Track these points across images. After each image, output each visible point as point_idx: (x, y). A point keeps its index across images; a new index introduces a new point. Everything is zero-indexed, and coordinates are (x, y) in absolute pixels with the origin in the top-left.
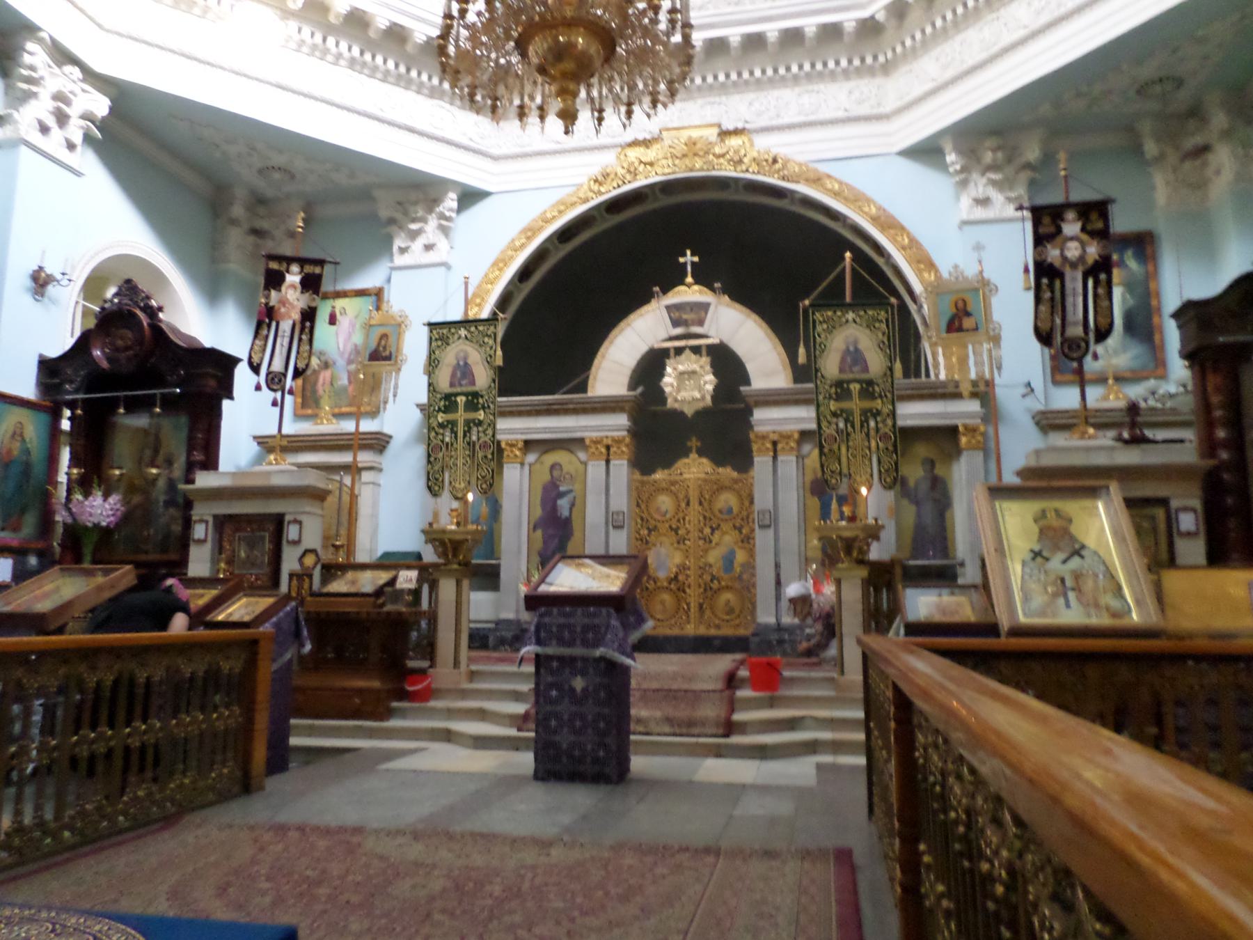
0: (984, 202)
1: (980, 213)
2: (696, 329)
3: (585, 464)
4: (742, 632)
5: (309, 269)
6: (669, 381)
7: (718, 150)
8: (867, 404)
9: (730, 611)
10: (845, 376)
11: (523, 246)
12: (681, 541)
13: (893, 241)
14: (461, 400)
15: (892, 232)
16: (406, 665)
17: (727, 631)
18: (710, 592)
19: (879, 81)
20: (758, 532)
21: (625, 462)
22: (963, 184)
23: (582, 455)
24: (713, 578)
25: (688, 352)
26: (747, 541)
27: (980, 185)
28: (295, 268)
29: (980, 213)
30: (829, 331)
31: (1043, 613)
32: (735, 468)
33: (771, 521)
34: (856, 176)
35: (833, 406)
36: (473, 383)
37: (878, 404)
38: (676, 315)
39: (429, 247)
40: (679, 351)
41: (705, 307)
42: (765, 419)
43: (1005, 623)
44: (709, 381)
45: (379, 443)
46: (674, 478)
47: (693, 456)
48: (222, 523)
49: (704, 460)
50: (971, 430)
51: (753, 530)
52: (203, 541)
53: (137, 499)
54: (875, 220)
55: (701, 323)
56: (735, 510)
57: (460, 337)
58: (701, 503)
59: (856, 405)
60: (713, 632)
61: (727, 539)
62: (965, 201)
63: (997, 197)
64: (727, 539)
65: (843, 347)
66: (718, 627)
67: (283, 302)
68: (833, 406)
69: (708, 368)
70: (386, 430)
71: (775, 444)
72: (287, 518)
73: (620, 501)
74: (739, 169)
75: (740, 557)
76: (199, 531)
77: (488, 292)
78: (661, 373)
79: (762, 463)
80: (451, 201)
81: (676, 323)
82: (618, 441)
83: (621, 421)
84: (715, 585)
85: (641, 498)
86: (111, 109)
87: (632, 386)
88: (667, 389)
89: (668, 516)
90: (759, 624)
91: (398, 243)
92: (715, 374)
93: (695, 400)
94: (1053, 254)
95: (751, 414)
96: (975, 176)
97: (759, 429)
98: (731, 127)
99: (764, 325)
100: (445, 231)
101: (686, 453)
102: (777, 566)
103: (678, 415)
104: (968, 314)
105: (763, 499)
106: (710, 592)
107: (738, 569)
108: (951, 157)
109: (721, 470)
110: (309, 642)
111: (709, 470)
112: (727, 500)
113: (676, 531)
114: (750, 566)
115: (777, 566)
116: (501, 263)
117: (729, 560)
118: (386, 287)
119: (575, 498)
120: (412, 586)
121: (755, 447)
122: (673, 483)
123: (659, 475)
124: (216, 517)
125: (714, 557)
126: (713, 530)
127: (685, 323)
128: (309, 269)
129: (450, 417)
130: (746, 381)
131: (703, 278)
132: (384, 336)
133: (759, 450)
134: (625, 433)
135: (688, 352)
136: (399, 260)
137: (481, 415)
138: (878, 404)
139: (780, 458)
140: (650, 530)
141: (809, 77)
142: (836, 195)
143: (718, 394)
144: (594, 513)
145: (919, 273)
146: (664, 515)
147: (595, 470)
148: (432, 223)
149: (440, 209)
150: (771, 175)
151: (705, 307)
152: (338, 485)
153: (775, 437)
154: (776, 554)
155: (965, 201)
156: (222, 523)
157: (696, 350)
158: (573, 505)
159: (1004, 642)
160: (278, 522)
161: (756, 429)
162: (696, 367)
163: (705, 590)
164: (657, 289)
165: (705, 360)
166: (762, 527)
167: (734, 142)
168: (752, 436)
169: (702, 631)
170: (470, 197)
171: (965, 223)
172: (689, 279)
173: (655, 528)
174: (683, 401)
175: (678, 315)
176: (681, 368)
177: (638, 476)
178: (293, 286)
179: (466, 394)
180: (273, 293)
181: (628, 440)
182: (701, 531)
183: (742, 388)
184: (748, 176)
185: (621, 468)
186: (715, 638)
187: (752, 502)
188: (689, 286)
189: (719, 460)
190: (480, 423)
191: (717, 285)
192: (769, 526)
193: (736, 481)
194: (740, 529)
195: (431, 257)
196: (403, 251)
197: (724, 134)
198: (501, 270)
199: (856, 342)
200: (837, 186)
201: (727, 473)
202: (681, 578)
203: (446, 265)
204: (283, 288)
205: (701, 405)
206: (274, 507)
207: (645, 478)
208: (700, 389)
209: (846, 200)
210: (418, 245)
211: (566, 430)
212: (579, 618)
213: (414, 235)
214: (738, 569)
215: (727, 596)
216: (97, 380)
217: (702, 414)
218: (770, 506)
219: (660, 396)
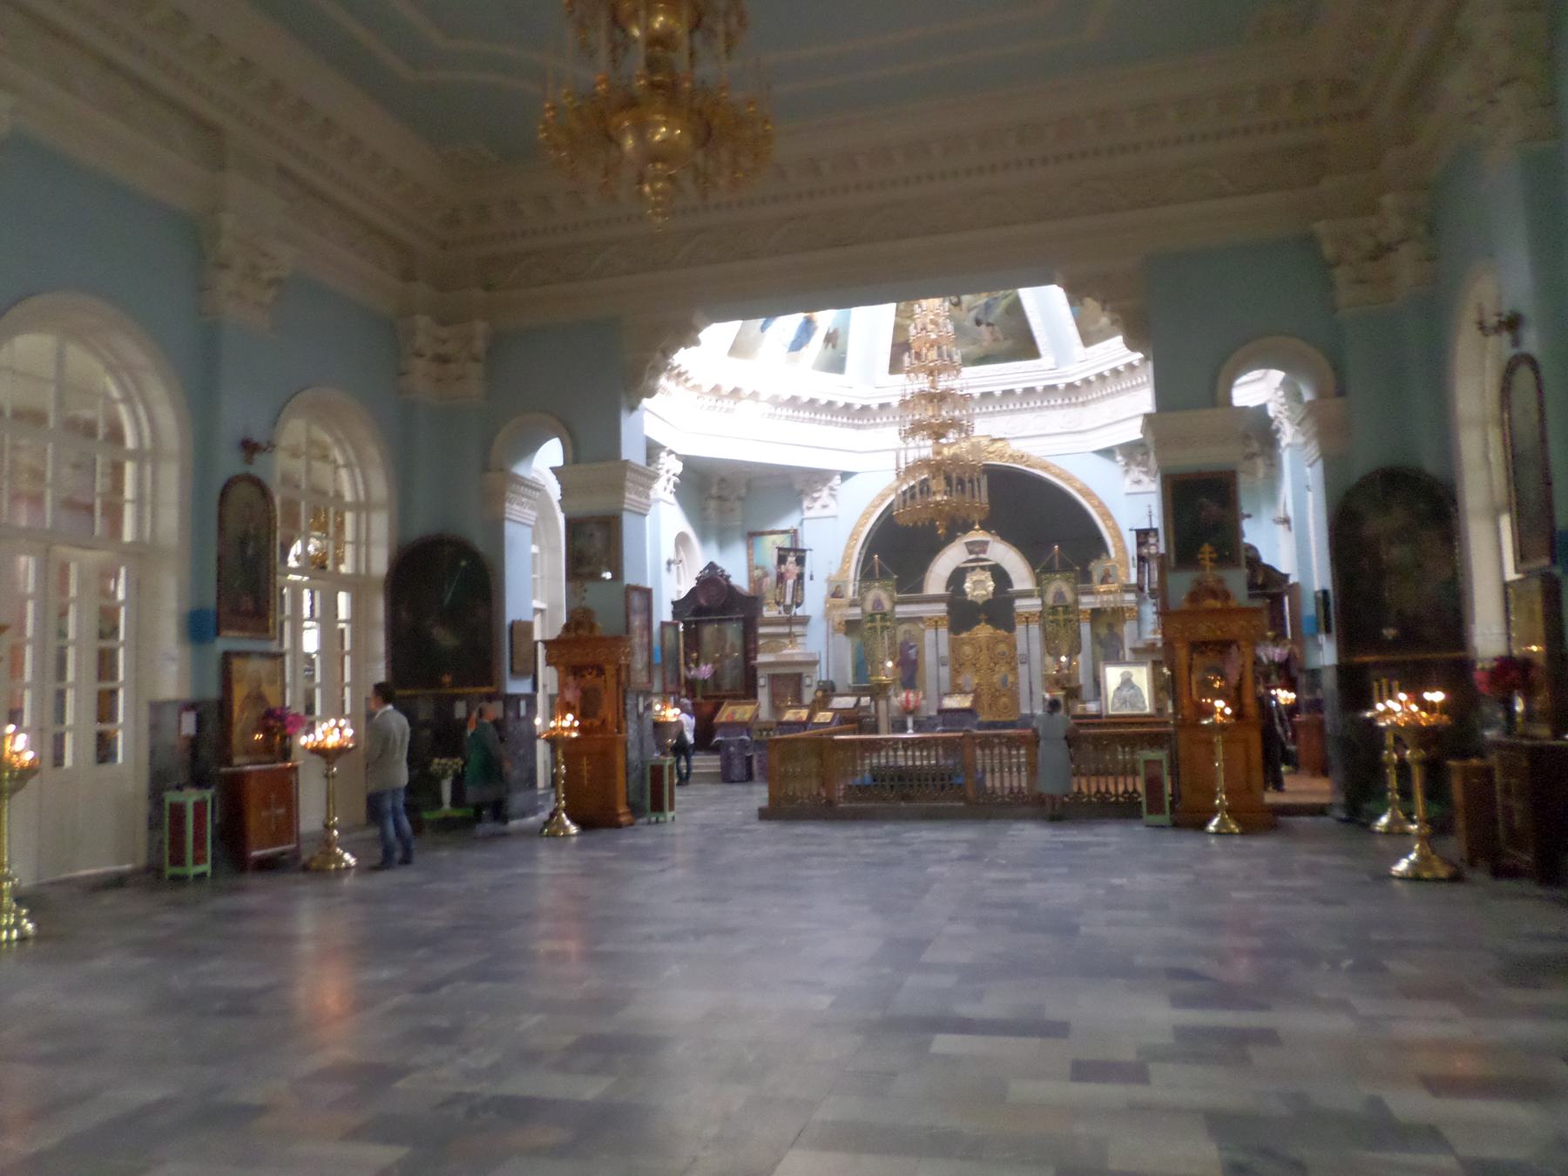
0: (1138, 482)
1: (1136, 488)
2: (982, 556)
3: (923, 630)
4: (1012, 718)
5: (798, 554)
6: (968, 586)
7: (991, 449)
8: (1066, 617)
9: (1006, 707)
10: (1056, 604)
11: (880, 504)
12: (978, 671)
13: (1089, 501)
14: (878, 617)
15: (1089, 497)
16: (1444, 691)
17: (1004, 718)
18: (994, 699)
19: (1080, 410)
20: (1019, 665)
21: (946, 630)
22: (1127, 472)
23: (921, 626)
24: (996, 690)
25: (978, 569)
26: (1014, 669)
27: (1136, 472)
28: (792, 554)
29: (1136, 488)
30: (1048, 583)
31: (1117, 710)
32: (1006, 630)
33: (1026, 660)
34: (1066, 464)
35: (1051, 618)
36: (883, 608)
37: (1071, 616)
38: (971, 548)
39: (825, 507)
40: (973, 569)
41: (986, 543)
42: (1022, 605)
43: (1104, 714)
44: (991, 585)
45: (804, 621)
46: (971, 636)
47: (983, 624)
48: (774, 678)
49: (989, 626)
50: (1131, 609)
51: (1017, 664)
52: (764, 686)
53: (718, 665)
54: (1079, 491)
55: (984, 552)
56: (1007, 653)
57: (875, 587)
58: (988, 650)
59: (1061, 617)
60: (997, 719)
61: (1003, 669)
62: (1128, 481)
63: (1145, 479)
64: (1003, 669)
65: (1055, 590)
66: (1000, 716)
67: (787, 571)
68: (1051, 618)
69: (990, 578)
70: (807, 614)
71: (1027, 618)
72: (805, 675)
73: (944, 650)
74: (1004, 460)
75: (1011, 679)
76: (762, 682)
77: (861, 532)
78: (963, 581)
79: (1020, 629)
80: (837, 479)
81: (971, 552)
82: (941, 618)
83: (943, 607)
84: (997, 694)
85: (955, 647)
86: (684, 467)
87: (947, 588)
88: (968, 590)
89: (970, 657)
90: (1022, 714)
91: (806, 503)
92: (993, 581)
93: (984, 595)
94: (1145, 551)
95: (1013, 603)
96: (1133, 467)
97: (1018, 610)
98: (997, 437)
99: (1020, 553)
100: (833, 496)
101: (978, 623)
102: (1030, 683)
103: (973, 604)
104: (1110, 576)
105: (1021, 648)
106: (994, 699)
107: (1010, 685)
108: (1119, 458)
109: (998, 631)
110: (1229, 722)
111: (992, 631)
112: (1002, 647)
113: (975, 665)
114: (1015, 684)
115: (1030, 683)
116: (866, 515)
117: (1004, 681)
118: (799, 528)
119: (1108, 453)
120: (868, 704)
121: (1016, 621)
122: (973, 639)
123: (964, 635)
124: (769, 675)
125: (996, 678)
126: (995, 664)
127: (977, 553)
128: (798, 554)
129: (873, 624)
130: (1011, 586)
131: (985, 526)
132: (838, 587)
133: (1019, 622)
134: (945, 614)
135: (978, 569)
136: (807, 514)
137: (888, 624)
138: (1071, 616)
139: (1031, 626)
140: (960, 665)
141: (1040, 408)
142: (1057, 476)
143: (995, 591)
144: (929, 657)
145: (1104, 521)
146: (968, 656)
147: (929, 635)
148: (825, 492)
149: (830, 484)
150: (1021, 464)
151: (986, 543)
152: (51, 391)
153: (1027, 615)
154: (1030, 678)
155: (1128, 481)
156: (774, 678)
157: (983, 568)
158: (917, 653)
159: (1104, 720)
160: (799, 677)
161: (1018, 610)
162: (983, 577)
163: (992, 697)
164: (959, 534)
165: (988, 574)
166: (1022, 663)
167: (999, 444)
168: (1015, 615)
169: (991, 719)
170: (846, 476)
171: (1128, 494)
172: (977, 527)
173: (963, 664)
174: (977, 596)
175: (971, 547)
176: (975, 578)
177: (952, 636)
178: (791, 563)
179: (881, 614)
180: (783, 566)
181: (947, 618)
182: (989, 665)
183: (1010, 590)
184: (1007, 464)
185: (944, 632)
186: (999, 722)
187: (1016, 649)
188: (977, 530)
189: (997, 626)
190: (888, 628)
191: (993, 532)
192: (1025, 663)
193: (1007, 638)
194: (1009, 663)
195: (826, 512)
196: (809, 508)
197: (995, 440)
198: (867, 519)
199: (1060, 589)
200: (1058, 471)
201: (1002, 633)
202: (979, 690)
203: (835, 517)
204: (787, 563)
205: (985, 599)
206: (798, 670)
207: (957, 637)
208: (986, 590)
209: (1062, 479)
210: (818, 505)
211: (913, 613)
212: (957, 717)
213: (815, 500)
214: (1010, 685)
215: (1004, 700)
216: (699, 611)
217: (987, 603)
218: (1025, 652)
219: (964, 593)
